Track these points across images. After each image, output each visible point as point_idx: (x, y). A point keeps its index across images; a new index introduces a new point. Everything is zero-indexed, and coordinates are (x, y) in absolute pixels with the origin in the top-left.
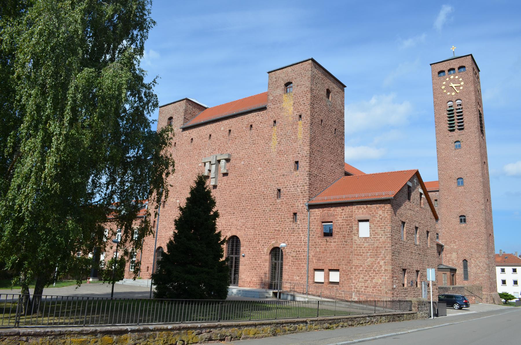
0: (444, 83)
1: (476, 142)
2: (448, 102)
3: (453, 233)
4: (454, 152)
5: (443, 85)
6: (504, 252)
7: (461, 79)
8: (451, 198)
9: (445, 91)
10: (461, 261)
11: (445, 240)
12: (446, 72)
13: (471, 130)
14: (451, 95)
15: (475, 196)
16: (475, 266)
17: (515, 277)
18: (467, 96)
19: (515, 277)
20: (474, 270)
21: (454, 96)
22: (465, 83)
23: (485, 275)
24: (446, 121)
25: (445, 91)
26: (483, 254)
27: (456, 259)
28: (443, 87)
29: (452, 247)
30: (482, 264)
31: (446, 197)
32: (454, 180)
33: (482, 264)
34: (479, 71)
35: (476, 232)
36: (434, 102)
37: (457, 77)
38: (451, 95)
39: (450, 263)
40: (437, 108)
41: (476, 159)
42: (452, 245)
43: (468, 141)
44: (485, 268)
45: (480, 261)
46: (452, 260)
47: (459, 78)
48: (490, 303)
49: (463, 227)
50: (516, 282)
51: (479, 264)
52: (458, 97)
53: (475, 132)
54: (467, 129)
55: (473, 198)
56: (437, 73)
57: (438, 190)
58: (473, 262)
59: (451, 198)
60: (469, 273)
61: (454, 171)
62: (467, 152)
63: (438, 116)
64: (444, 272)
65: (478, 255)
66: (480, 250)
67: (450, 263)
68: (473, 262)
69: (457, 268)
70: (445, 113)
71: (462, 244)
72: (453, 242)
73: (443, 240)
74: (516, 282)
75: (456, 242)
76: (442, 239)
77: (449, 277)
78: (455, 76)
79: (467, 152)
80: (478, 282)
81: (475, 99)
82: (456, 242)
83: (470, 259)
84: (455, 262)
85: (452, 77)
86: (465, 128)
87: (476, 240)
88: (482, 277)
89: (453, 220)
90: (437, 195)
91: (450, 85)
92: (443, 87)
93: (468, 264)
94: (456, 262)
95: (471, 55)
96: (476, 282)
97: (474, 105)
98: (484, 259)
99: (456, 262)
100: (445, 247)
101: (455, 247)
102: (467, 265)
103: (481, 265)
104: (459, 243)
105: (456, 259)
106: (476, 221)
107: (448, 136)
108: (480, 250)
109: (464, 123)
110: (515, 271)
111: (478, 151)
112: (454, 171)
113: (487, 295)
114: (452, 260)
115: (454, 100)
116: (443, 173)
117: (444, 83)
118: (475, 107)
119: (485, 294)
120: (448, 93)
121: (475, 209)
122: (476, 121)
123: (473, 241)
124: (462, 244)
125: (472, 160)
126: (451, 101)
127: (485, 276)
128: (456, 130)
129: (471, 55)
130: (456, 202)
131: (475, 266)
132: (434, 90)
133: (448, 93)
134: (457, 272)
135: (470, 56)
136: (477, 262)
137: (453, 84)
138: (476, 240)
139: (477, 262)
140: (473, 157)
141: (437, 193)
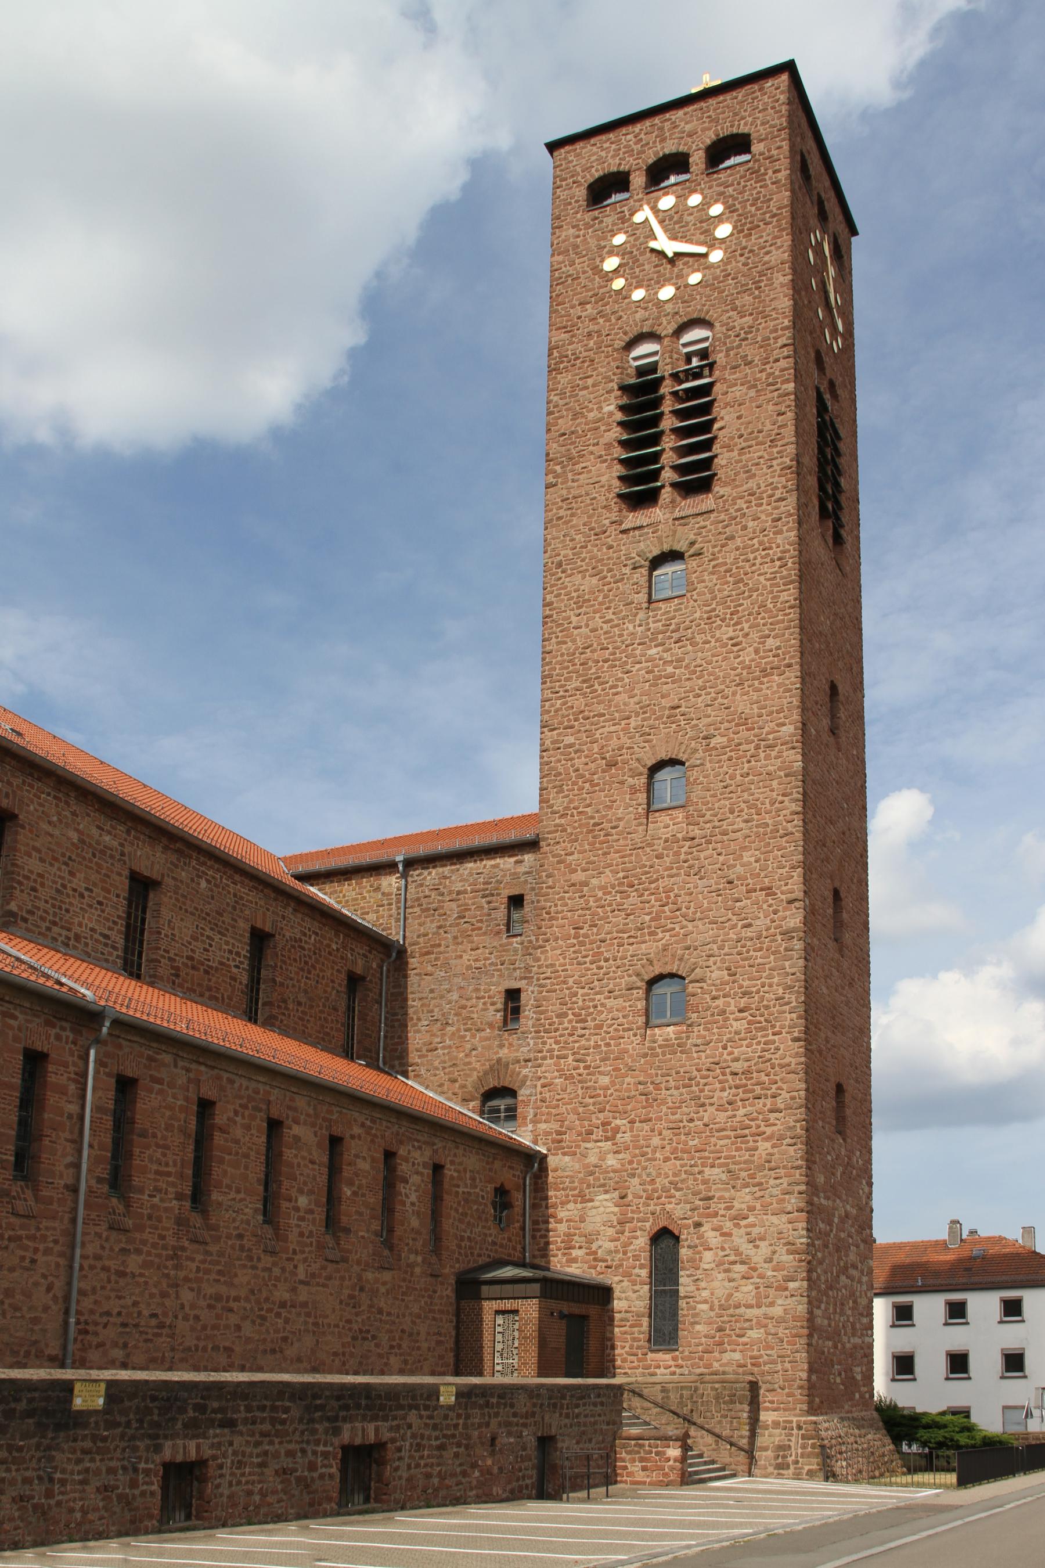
0: (619, 239)
1: (775, 552)
2: (630, 345)
3: (605, 1080)
4: (641, 615)
5: (613, 251)
6: (973, 1232)
7: (716, 210)
8: (608, 877)
9: (618, 284)
10: (642, 1241)
11: (555, 1126)
12: (638, 180)
13: (752, 484)
14: (651, 300)
15: (748, 856)
16: (724, 1266)
17: (1012, 1336)
18: (747, 299)
19: (1012, 1336)
20: (718, 1286)
21: (669, 308)
22: (738, 230)
23: (777, 1311)
24: (608, 446)
25: (618, 284)
26: (775, 1188)
27: (611, 1232)
28: (611, 263)
29: (592, 1159)
30: (765, 1249)
31: (579, 876)
32: (635, 774)
33: (765, 1249)
34: (854, 231)
35: (737, 1066)
36: (550, 351)
37: (695, 200)
38: (651, 300)
39: (575, 1253)
40: (564, 379)
41: (771, 643)
42: (595, 1151)
43: (731, 545)
44: (780, 1275)
45: (756, 1231)
46: (590, 1238)
47: (706, 205)
48: (797, 1477)
49: (667, 1045)
50: (1014, 1362)
51: (746, 1248)
52: (693, 311)
53: (778, 494)
54: (731, 482)
55: (739, 869)
56: (581, 193)
57: (529, 836)
58: (713, 1238)
59: (608, 877)
60: (682, 1303)
61: (633, 722)
62: (720, 610)
63: (564, 424)
64: (508, 1305)
65: (743, 1198)
66: (761, 1168)
67: (575, 1253)
68: (713, 1238)
69: (611, 1279)
70: (611, 407)
71: (656, 1141)
72: (599, 1133)
73: (543, 1126)
74: (1014, 1362)
75: (616, 1130)
76: (535, 1121)
77: (532, 1330)
78: (682, 198)
79: (720, 610)
80: (737, 1356)
81: (789, 312)
82: (616, 1130)
83: (698, 1225)
84: (604, 1245)
85: (667, 202)
86: (721, 474)
87: (742, 1112)
88: (760, 1325)
89: (610, 1003)
90: (522, 869)
91: (653, 244)
92: (611, 263)
93: (684, 1252)
94: (611, 1245)
95: (789, 68)
96: (727, 1357)
97: (781, 342)
98: (780, 1222)
99: (611, 1245)
100: (552, 1161)
101: (611, 1161)
102: (675, 1259)
103: (759, 1255)
104: (635, 1139)
105: (611, 1232)
106: (743, 1003)
107: (612, 530)
108: (761, 1168)
109: (716, 448)
110: (1012, 1309)
111: (784, 596)
112: (633, 722)
113: (787, 1426)
114: (590, 1238)
115: (667, 328)
116: (570, 740)
117: (619, 239)
118: (786, 351)
119: (776, 1424)
120: (638, 294)
121: (749, 933)
122: (789, 432)
123: (721, 1117)
124: (656, 1141)
125: (748, 656)
126: (651, 336)
127: (780, 1321)
128: (666, 494)
129: (789, 68)
130: (634, 898)
131: (724, 1266)
132: (556, 282)
133: (638, 294)
134: (617, 1304)
135: (785, 77)
136: (739, 1239)
137: (673, 238)
138: (742, 1112)
139: (739, 1239)
140: (754, 636)
141: (528, 858)
